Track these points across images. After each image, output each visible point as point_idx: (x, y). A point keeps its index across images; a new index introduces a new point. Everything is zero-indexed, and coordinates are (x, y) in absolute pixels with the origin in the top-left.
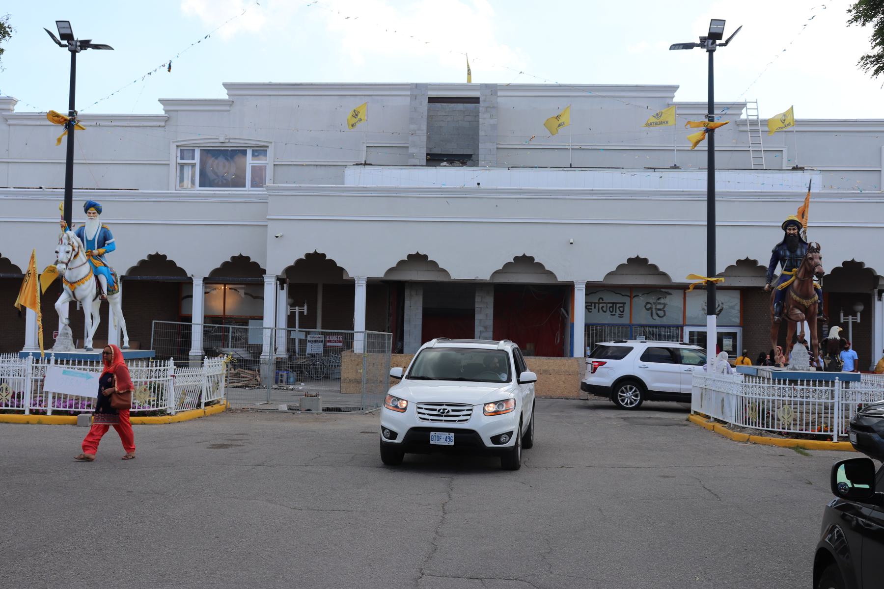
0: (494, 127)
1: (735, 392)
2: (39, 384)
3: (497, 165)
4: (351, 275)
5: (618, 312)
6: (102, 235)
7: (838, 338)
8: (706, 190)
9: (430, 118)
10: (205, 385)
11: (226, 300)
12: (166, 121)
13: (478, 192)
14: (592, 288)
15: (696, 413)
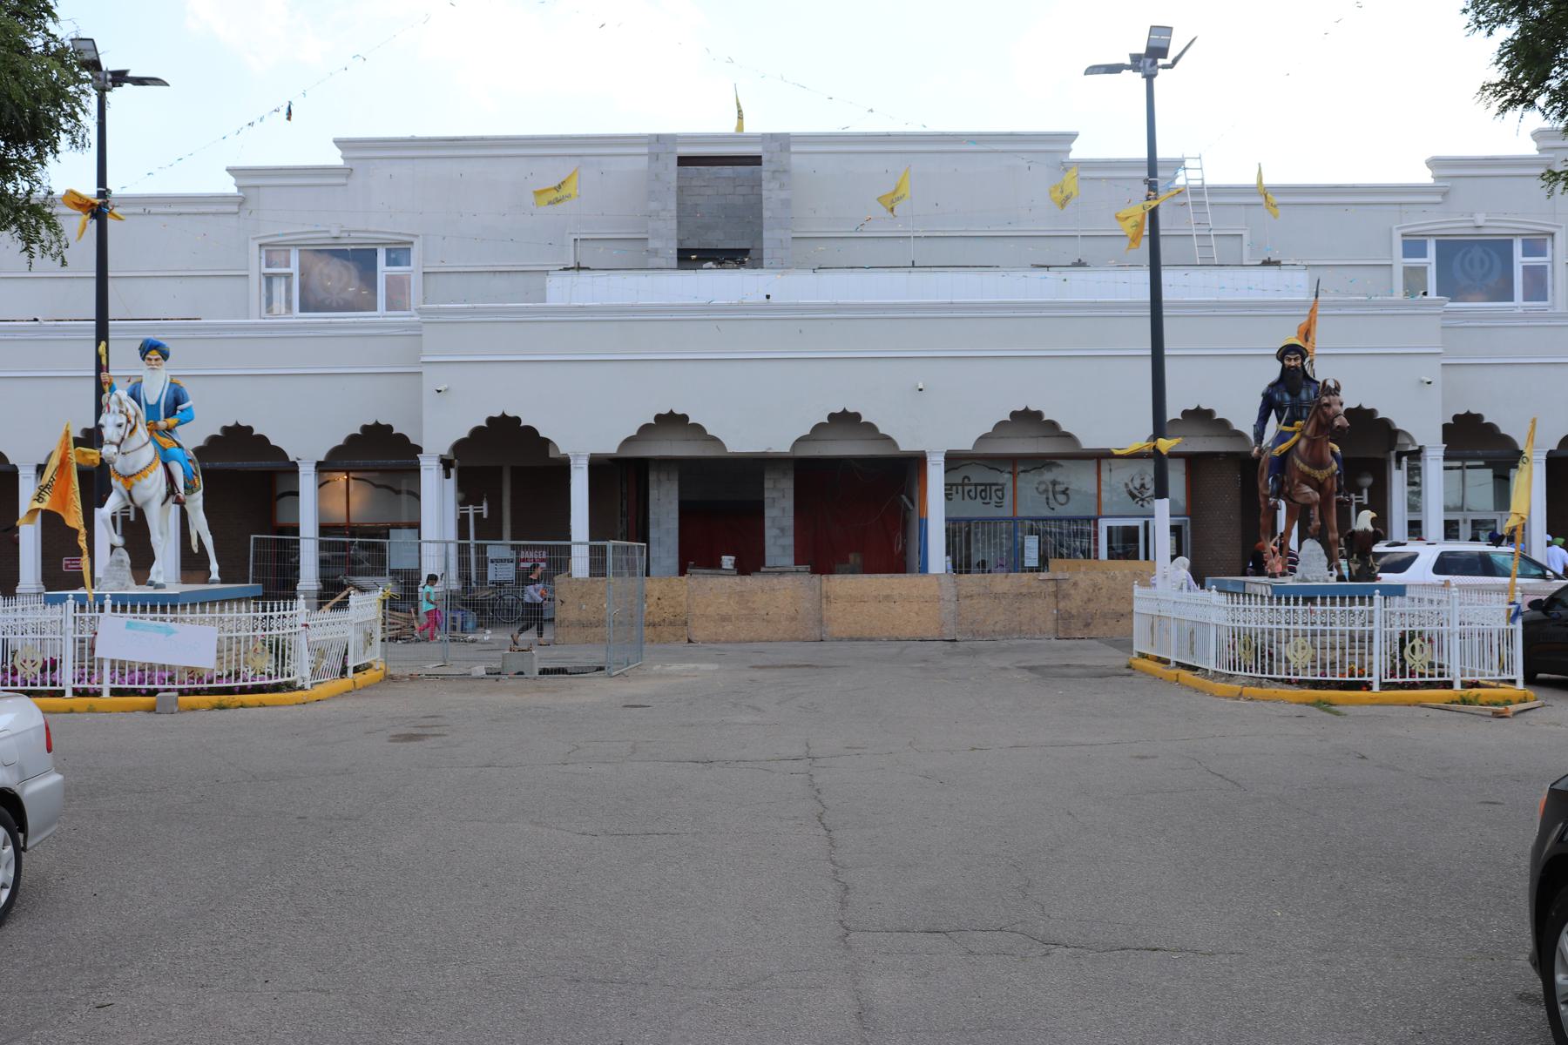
0: (786, 203)
1: (1214, 620)
2: (86, 648)
3: (784, 266)
4: (562, 451)
5: (994, 498)
6: (172, 396)
7: (1371, 528)
8: (1148, 298)
9: (680, 189)
10: (354, 638)
11: (354, 500)
12: (240, 204)
13: (767, 310)
14: (954, 461)
15: (1143, 656)
